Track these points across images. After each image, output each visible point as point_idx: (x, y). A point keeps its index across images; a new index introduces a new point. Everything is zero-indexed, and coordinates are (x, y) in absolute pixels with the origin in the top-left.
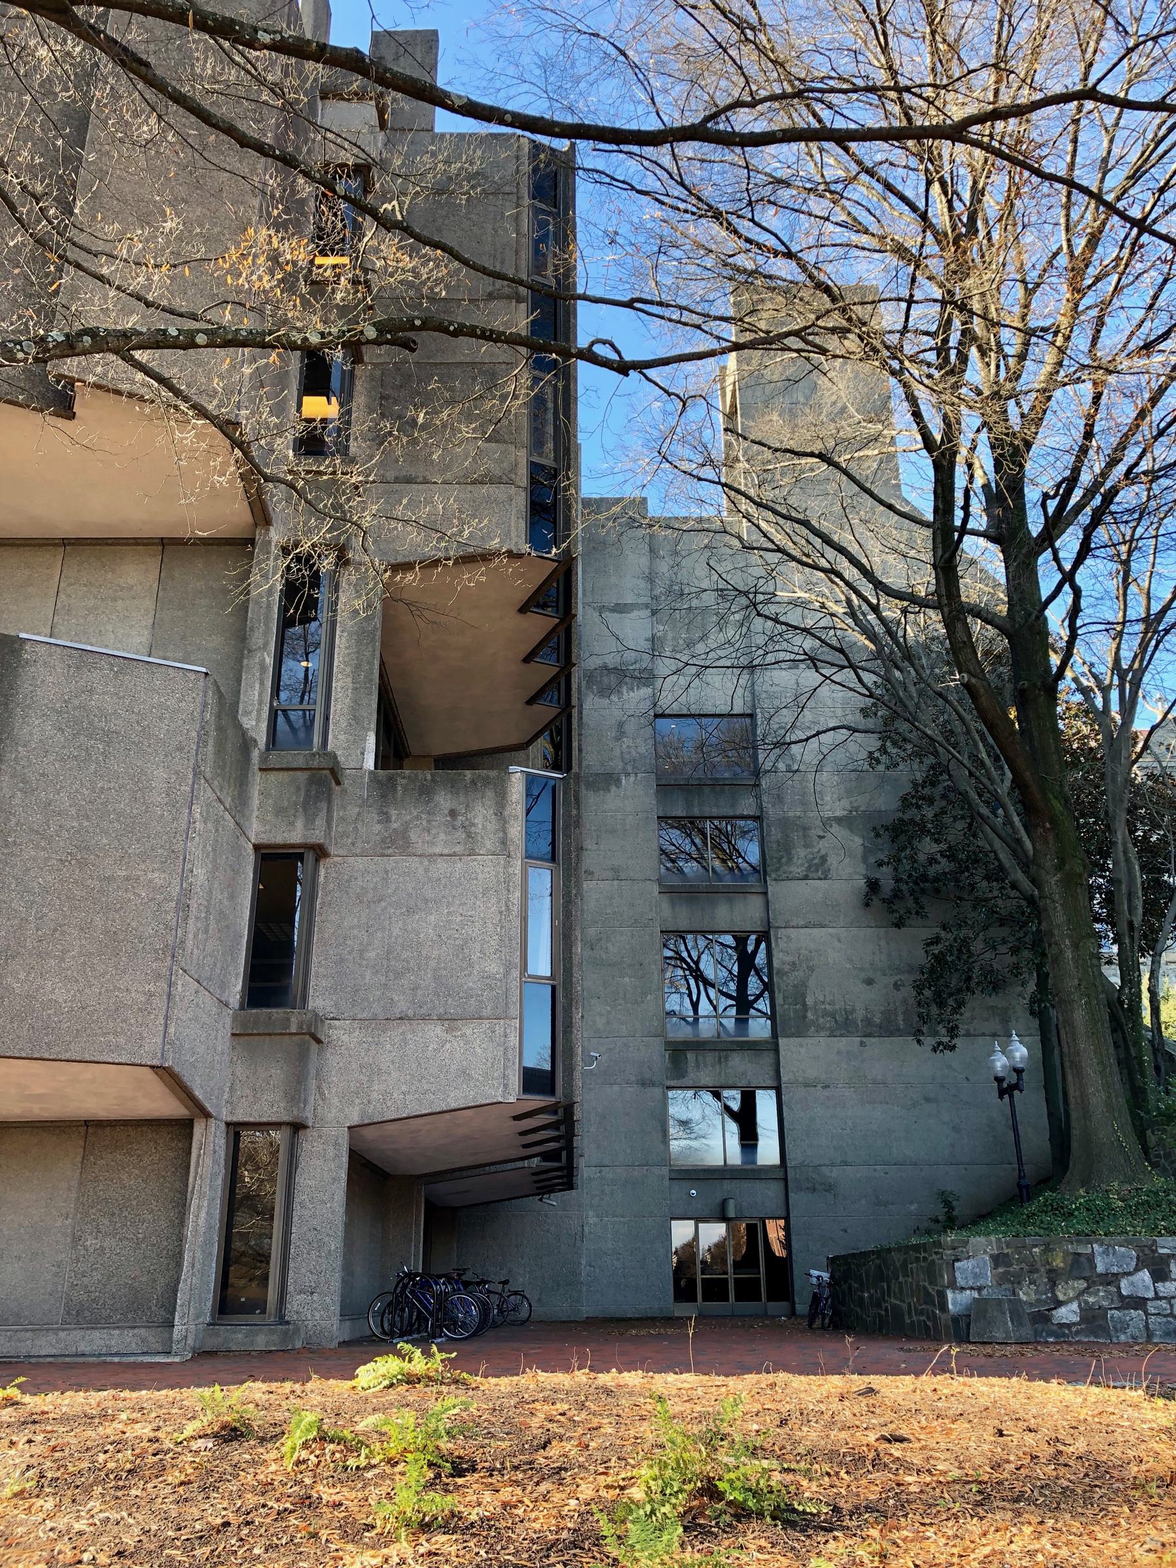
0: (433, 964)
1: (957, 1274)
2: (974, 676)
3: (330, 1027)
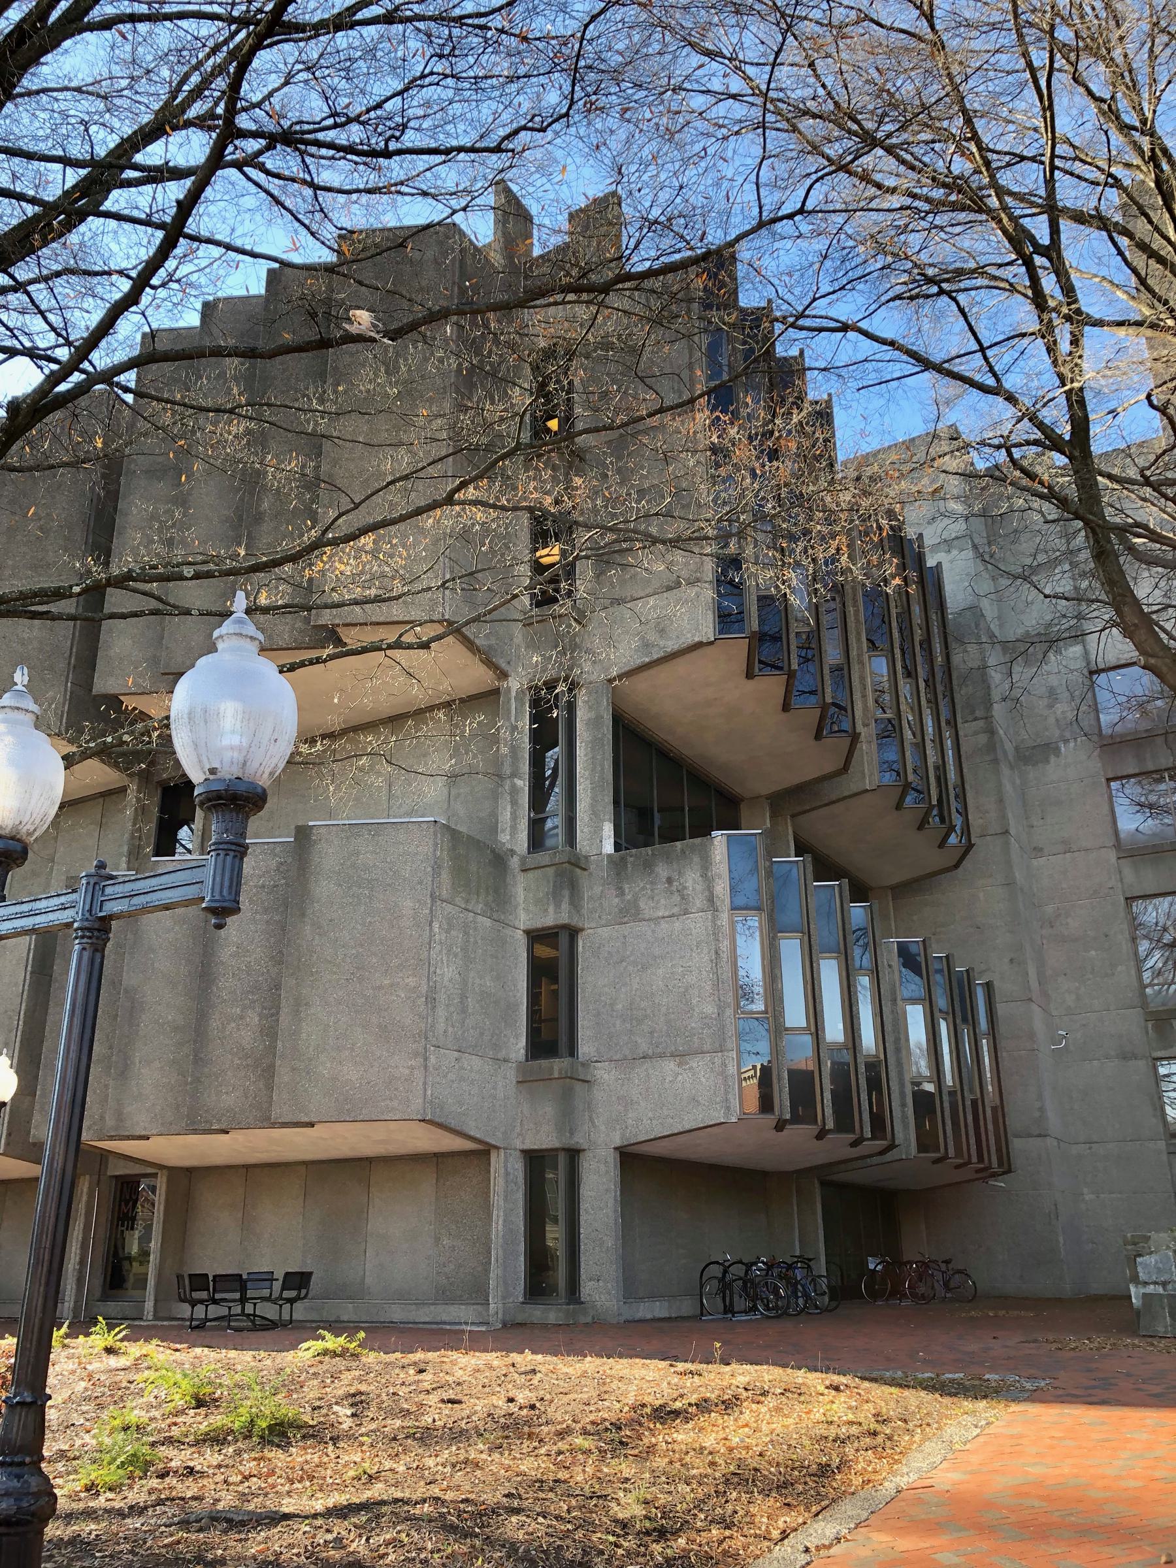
0: (664, 1009)
1: (1139, 1269)
2: (1152, 656)
3: (595, 1068)
